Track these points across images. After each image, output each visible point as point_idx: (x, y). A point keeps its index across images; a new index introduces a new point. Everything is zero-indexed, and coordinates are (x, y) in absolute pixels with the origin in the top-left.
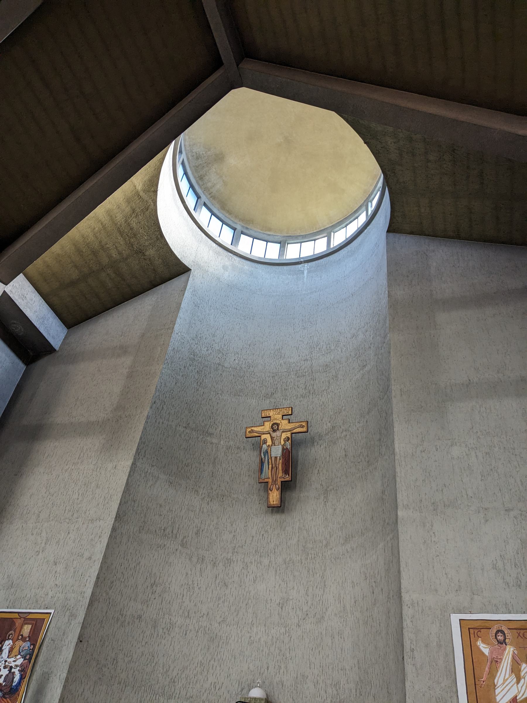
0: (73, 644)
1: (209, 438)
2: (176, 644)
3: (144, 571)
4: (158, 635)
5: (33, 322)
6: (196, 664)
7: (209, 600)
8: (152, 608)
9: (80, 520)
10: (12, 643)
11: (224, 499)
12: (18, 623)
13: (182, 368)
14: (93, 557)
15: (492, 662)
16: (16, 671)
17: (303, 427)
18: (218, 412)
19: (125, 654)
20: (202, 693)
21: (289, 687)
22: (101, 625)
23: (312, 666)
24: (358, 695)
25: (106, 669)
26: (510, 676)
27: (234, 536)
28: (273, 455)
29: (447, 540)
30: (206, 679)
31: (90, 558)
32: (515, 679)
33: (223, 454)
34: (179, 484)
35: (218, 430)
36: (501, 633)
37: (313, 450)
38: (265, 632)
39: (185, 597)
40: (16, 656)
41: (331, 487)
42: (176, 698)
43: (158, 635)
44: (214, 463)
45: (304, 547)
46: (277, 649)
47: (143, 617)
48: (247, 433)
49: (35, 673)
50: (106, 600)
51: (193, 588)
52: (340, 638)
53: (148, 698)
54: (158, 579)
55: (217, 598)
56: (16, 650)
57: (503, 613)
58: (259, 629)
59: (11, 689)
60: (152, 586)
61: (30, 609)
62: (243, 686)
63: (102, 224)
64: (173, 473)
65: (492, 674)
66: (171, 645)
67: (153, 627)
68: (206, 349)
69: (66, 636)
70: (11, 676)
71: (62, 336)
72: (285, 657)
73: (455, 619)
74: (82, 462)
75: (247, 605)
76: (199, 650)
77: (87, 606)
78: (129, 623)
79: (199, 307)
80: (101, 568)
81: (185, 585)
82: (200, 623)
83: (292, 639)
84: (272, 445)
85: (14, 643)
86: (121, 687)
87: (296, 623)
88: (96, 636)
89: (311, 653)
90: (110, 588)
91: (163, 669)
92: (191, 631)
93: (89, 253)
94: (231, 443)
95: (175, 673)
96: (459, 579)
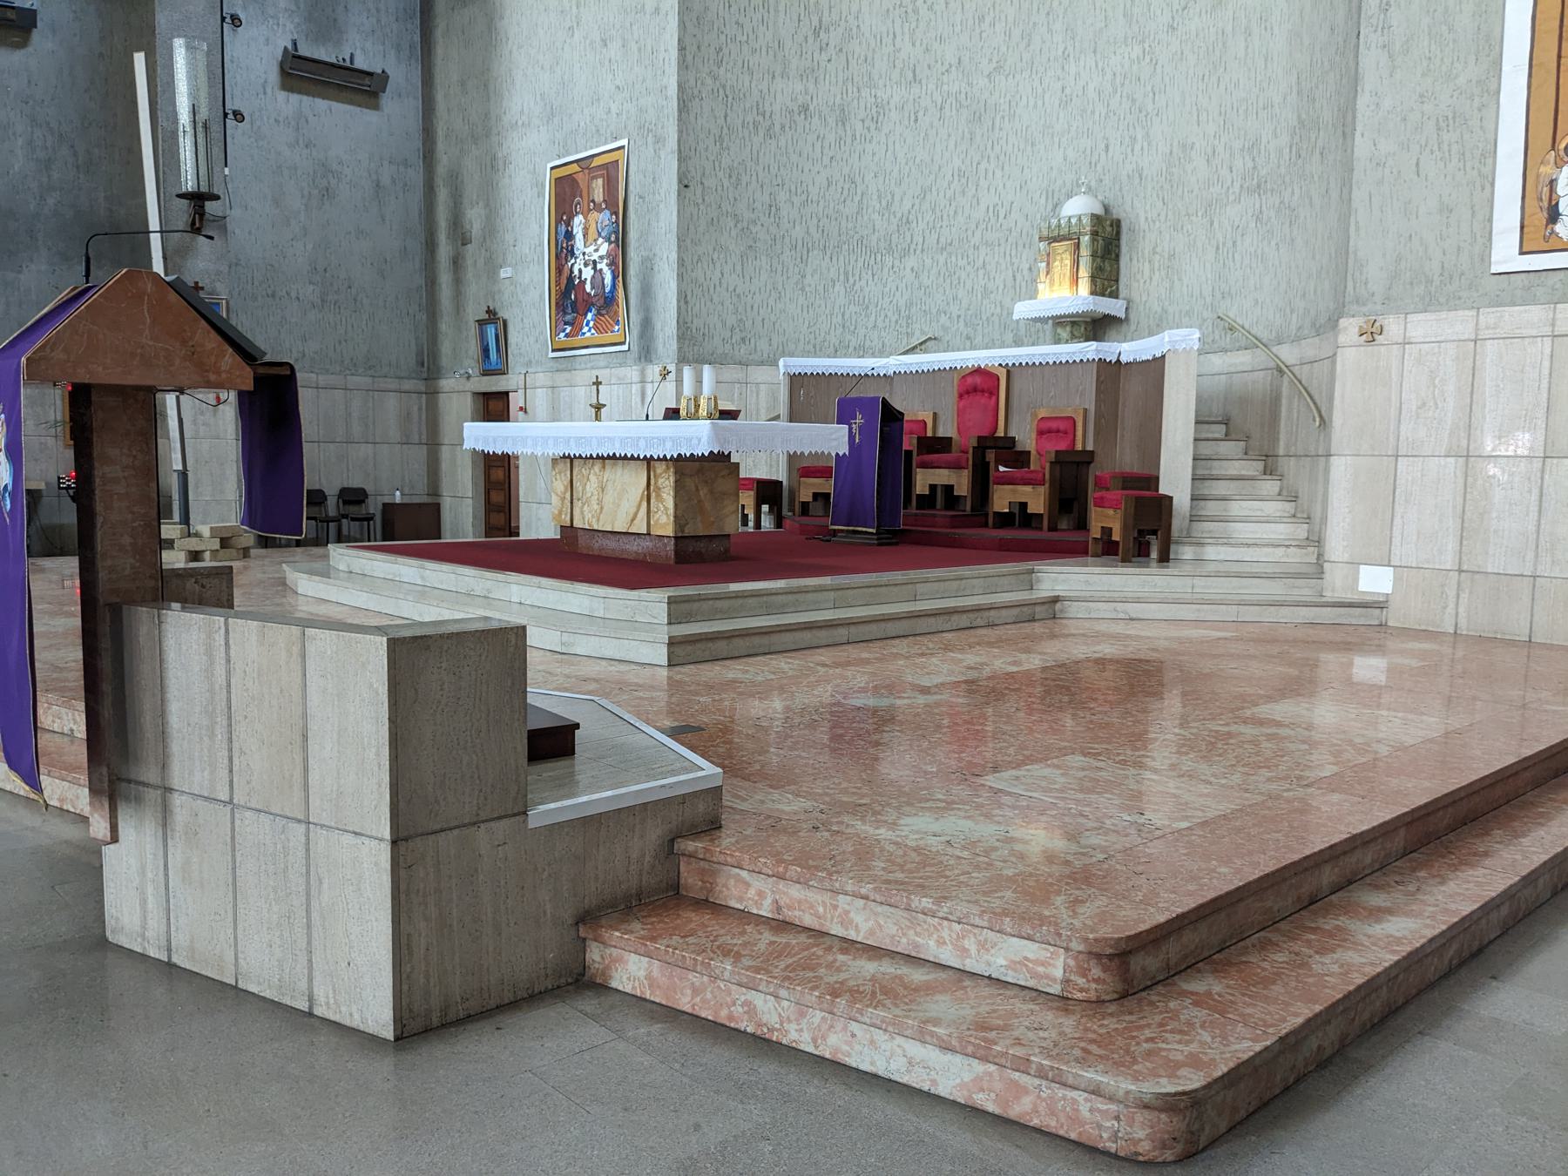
0: (674, 195)
2: (897, 145)
3: (788, 4)
4: (854, 136)
6: (948, 176)
7: (958, 29)
8: (827, 82)
10: (583, 221)
12: (582, 179)
14: (661, 5)
16: (603, 266)
19: (790, 191)
20: (970, 233)
21: (1155, 179)
22: (721, 145)
23: (1203, 117)
24: (1293, 158)
25: (759, 227)
30: (975, 201)
38: (1097, 66)
39: (899, 39)
40: (595, 240)
42: (918, 252)
46: (1124, 99)
47: (811, 108)
49: (631, 264)
50: (716, 90)
51: (916, 11)
52: (1263, 32)
53: (860, 264)
55: (976, 17)
56: (592, 230)
58: (1082, 63)
59: (606, 298)
60: (816, 33)
61: (591, 148)
62: (1055, 200)
66: (887, 151)
67: (840, 124)
69: (658, 184)
72: (1144, 113)
75: (1048, 14)
76: (951, 146)
77: (676, 114)
78: (783, 127)
80: (682, 25)
81: (894, 9)
82: (945, 87)
83: (1159, 70)
85: (585, 218)
86: (799, 255)
87: (1166, 25)
88: (717, 169)
89: (1200, 89)
90: (719, 64)
91: (880, 202)
92: (926, 110)
95: (907, 205)
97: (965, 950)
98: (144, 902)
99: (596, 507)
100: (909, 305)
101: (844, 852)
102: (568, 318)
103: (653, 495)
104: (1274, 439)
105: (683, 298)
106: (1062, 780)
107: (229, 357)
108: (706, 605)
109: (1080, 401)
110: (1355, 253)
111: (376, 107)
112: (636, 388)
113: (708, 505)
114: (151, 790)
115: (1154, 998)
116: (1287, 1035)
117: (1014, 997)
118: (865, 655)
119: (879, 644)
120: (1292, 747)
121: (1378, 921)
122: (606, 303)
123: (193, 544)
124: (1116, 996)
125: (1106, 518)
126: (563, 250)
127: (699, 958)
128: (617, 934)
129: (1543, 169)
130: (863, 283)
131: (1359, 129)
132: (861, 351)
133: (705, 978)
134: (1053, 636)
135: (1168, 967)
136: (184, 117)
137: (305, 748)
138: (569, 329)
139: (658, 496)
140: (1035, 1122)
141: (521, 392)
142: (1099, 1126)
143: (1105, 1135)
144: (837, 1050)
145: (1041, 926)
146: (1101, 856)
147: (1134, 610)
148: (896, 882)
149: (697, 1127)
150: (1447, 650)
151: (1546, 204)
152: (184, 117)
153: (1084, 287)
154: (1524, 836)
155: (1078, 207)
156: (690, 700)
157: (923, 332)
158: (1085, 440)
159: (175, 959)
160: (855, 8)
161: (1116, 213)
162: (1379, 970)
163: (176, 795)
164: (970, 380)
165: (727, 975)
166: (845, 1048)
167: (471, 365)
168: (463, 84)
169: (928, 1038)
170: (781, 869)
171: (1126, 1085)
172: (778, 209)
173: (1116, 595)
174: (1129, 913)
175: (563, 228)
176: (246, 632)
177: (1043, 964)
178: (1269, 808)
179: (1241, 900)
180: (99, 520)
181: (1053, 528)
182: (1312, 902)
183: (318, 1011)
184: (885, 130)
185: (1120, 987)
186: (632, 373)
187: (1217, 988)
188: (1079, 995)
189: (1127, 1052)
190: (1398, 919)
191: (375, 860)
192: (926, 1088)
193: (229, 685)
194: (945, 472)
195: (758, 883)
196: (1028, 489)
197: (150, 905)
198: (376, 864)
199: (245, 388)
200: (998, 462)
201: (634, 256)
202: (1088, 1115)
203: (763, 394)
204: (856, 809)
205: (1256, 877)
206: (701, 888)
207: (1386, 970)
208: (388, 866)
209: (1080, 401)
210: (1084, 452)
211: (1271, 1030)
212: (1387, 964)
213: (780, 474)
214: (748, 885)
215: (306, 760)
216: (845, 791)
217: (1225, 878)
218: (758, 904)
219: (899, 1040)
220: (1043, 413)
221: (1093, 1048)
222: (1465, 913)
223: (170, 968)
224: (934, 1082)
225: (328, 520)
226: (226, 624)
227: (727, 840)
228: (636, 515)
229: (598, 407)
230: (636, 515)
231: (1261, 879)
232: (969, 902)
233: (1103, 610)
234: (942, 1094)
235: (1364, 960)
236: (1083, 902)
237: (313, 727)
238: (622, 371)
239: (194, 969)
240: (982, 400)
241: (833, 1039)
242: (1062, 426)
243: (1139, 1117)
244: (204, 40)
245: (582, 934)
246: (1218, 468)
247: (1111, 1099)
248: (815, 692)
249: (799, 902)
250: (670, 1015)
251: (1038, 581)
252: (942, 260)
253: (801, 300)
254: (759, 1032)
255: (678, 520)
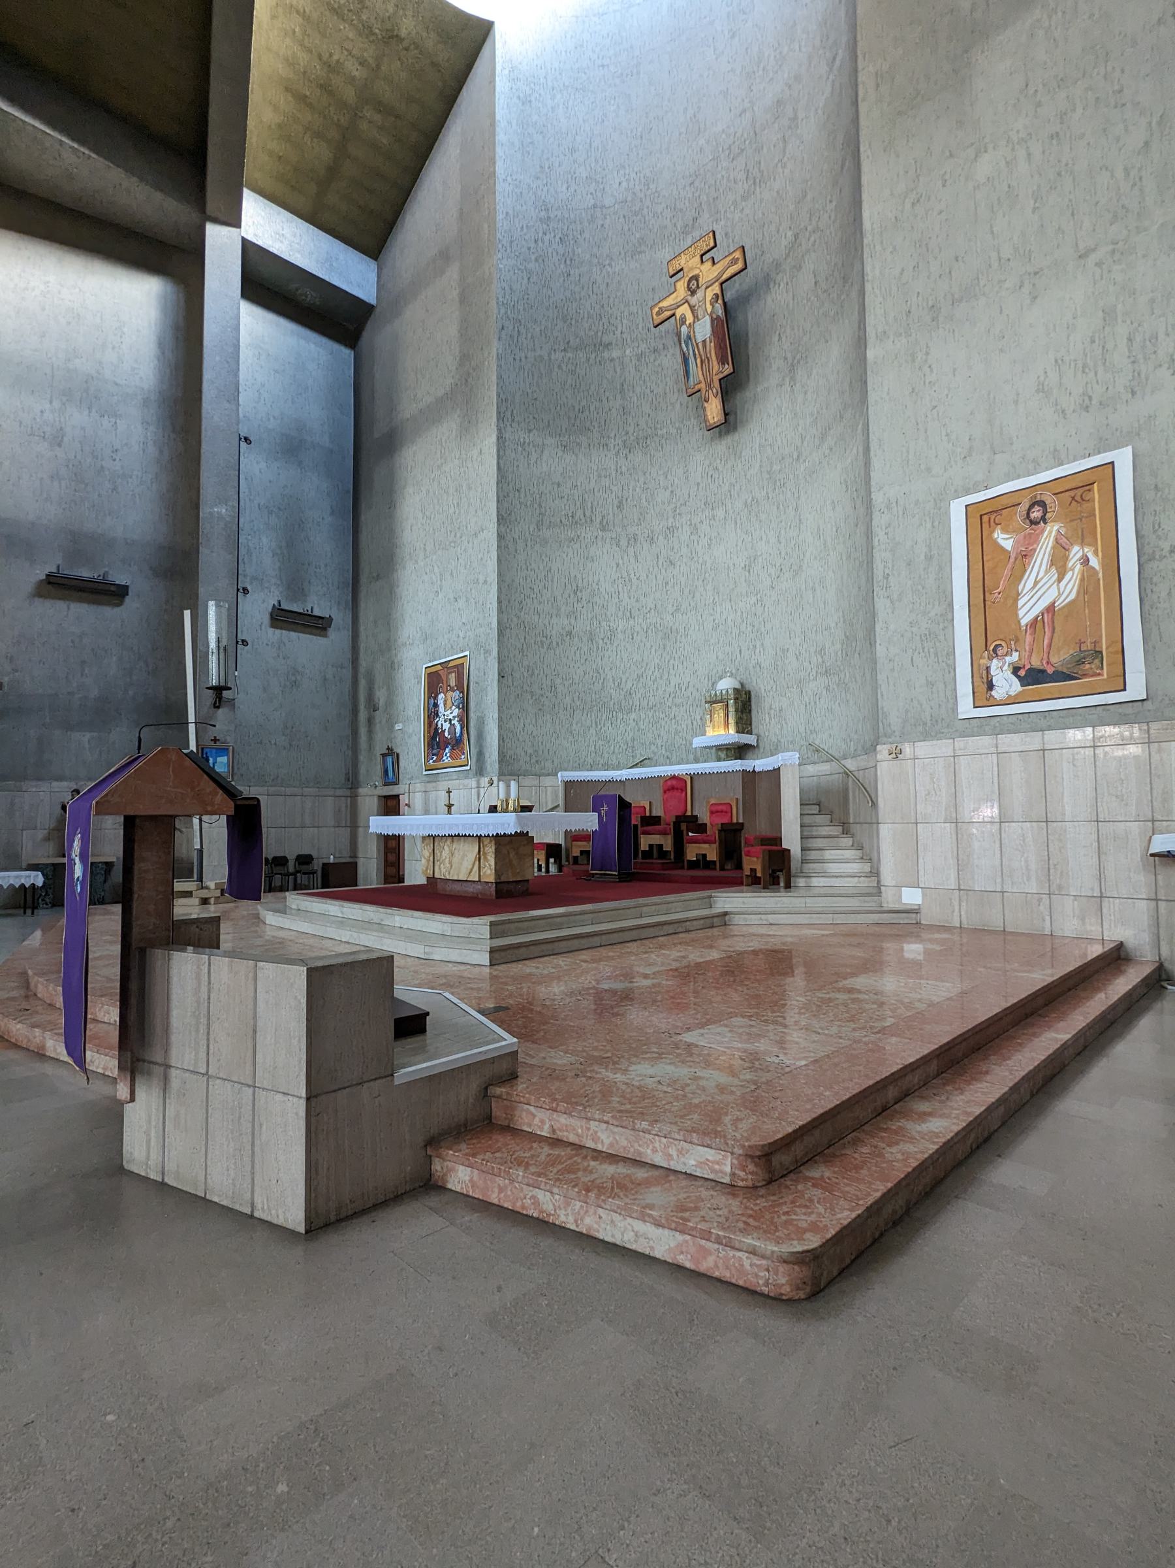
0: (496, 682)
1: (606, 354)
5: (314, 273)
7: (654, 589)
9: (463, 538)
11: (648, 442)
13: (532, 245)
15: (1016, 559)
16: (455, 722)
17: (734, 262)
18: (611, 300)
26: (1046, 572)
27: (672, 492)
28: (700, 339)
29: (955, 370)
31: (485, 582)
32: (1056, 575)
33: (633, 370)
34: (578, 444)
35: (618, 333)
36: (1039, 505)
37: (769, 300)
39: (621, 594)
41: (799, 356)
43: (598, 648)
44: (622, 391)
45: (769, 473)
48: (655, 316)
51: (630, 580)
54: (580, 581)
56: (449, 702)
57: (1047, 469)
60: (575, 593)
63: (298, 12)
64: (564, 431)
65: (1018, 575)
68: (565, 186)
70: (452, 728)
71: (373, 276)
73: (957, 510)
74: (445, 460)
78: (557, 644)
79: (530, 101)
80: (500, 590)
83: (766, 609)
84: (694, 322)
93: (318, 94)
94: (643, 346)
95: (629, 684)
96: (971, 436)
97: (670, 1155)
98: (148, 1142)
99: (448, 865)
100: (633, 740)
101: (594, 1092)
102: (435, 751)
103: (482, 857)
104: (847, 813)
105: (501, 739)
106: (729, 1035)
107: (220, 795)
108: (512, 926)
109: (734, 794)
110: (882, 708)
111: (325, 636)
112: (474, 791)
113: (515, 862)
114: (157, 1067)
115: (789, 1183)
116: (871, 1205)
117: (702, 1186)
118: (611, 954)
119: (619, 946)
120: (867, 1006)
121: (924, 1121)
122: (457, 743)
123: (204, 894)
124: (764, 1183)
125: (753, 863)
126: (432, 713)
127: (503, 1168)
128: (451, 1152)
129: (982, 661)
130: (606, 728)
131: (878, 642)
132: (607, 767)
133: (507, 1181)
134: (725, 937)
135: (797, 1161)
136: (213, 644)
137: (254, 1039)
138: (435, 758)
139: (486, 858)
140: (717, 1274)
141: (407, 795)
142: (757, 1276)
143: (761, 1282)
144: (590, 1228)
145: (716, 1138)
146: (753, 1087)
147: (772, 918)
148: (627, 1111)
149: (499, 1289)
150: (956, 938)
151: (985, 680)
152: (213, 644)
153: (732, 730)
154: (1009, 1058)
155: (726, 685)
156: (502, 989)
157: (641, 755)
158: (738, 817)
159: (166, 1180)
160: (596, 579)
161: (748, 687)
162: (926, 1156)
163: (173, 1070)
164: (669, 783)
165: (520, 1179)
166: (595, 1226)
167: (378, 781)
168: (375, 622)
169: (647, 1218)
170: (554, 1105)
171: (772, 1247)
172: (556, 688)
173: (760, 910)
174: (769, 1126)
175: (432, 701)
176: (220, 963)
177: (718, 1163)
178: (854, 1049)
179: (839, 1113)
180: (136, 896)
181: (722, 869)
182: (884, 1110)
183: (256, 1214)
184: (615, 644)
185: (767, 1177)
186: (472, 782)
187: (827, 1174)
188: (741, 1184)
189: (772, 1223)
190: (935, 1119)
191: (297, 1108)
192: (647, 1253)
193: (209, 998)
194: (658, 836)
195: (541, 1115)
196: (706, 846)
197: (152, 1144)
198: (297, 1114)
199: (229, 813)
200: (688, 830)
201: (473, 716)
202: (748, 1268)
203: (549, 793)
204: (602, 1061)
205: (847, 1097)
206: (506, 1119)
207: (931, 1156)
208: (304, 1114)
209: (734, 794)
210: (738, 823)
211: (861, 1202)
212: (931, 1152)
213: (561, 840)
214: (534, 1116)
215: (255, 1046)
216: (595, 1049)
217: (829, 1100)
218: (542, 1129)
219: (629, 1220)
220: (713, 801)
221: (751, 1221)
222: (977, 1114)
223: (162, 1186)
224: (652, 1248)
225: (288, 874)
226: (209, 959)
227: (521, 1086)
228: (472, 870)
229: (450, 806)
230: (472, 870)
231: (850, 1098)
232: (671, 1123)
233: (754, 919)
234: (657, 1256)
235: (916, 1150)
236: (741, 1120)
237: (260, 1024)
238: (466, 782)
239: (179, 1187)
240: (677, 793)
241: (588, 1220)
242: (723, 808)
243: (781, 1269)
244: (227, 601)
245: (429, 1153)
246: (815, 831)
247: (763, 1257)
248: (580, 981)
249: (566, 1126)
250: (484, 1207)
251: (715, 902)
252: (651, 715)
253: (571, 738)
254: (541, 1217)
255: (498, 872)
